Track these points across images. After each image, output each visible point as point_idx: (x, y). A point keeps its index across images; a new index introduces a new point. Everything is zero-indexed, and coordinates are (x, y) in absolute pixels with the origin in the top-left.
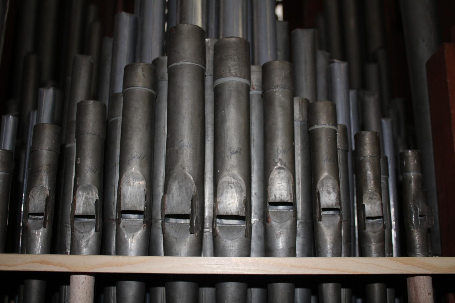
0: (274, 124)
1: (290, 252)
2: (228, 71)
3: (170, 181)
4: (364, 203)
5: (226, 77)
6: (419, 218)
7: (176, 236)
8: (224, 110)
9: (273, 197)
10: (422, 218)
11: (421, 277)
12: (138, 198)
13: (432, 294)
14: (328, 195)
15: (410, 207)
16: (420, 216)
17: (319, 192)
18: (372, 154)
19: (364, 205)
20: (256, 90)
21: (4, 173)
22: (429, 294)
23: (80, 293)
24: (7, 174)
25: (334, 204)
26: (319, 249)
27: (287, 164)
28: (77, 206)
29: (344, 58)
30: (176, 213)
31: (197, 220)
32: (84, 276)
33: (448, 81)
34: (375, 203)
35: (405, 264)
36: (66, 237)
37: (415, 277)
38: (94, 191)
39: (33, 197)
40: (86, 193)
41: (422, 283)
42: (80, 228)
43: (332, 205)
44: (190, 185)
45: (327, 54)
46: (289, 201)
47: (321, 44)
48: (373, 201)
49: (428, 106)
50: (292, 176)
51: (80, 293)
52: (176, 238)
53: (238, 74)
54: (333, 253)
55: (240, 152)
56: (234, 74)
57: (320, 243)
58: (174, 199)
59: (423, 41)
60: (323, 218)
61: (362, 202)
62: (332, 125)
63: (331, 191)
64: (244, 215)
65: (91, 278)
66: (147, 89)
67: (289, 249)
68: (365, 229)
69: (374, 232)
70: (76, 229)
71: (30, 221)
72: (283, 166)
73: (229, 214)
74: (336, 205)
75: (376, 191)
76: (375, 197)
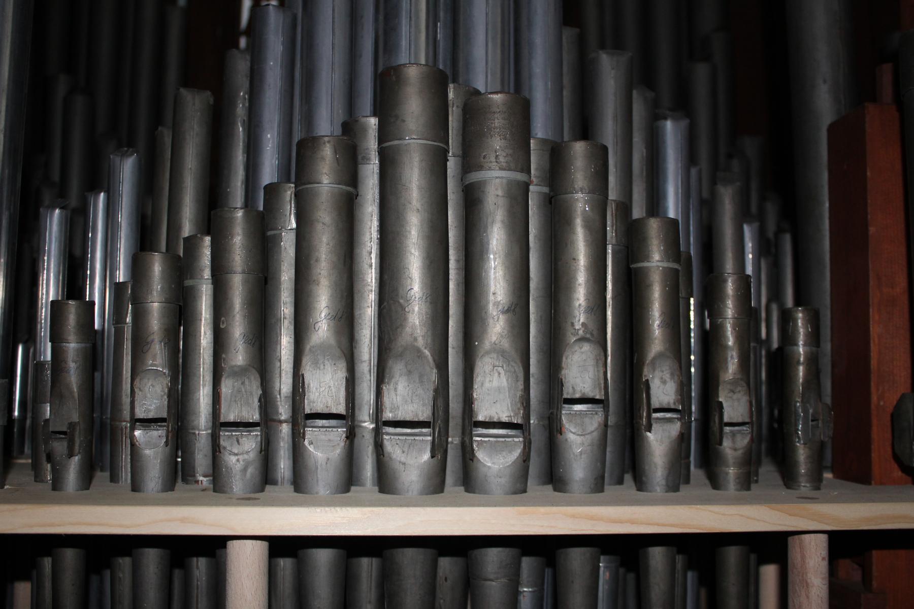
0: (574, 259)
1: (596, 484)
2: (493, 159)
3: (390, 363)
4: (720, 400)
5: (490, 169)
6: (810, 423)
7: (403, 459)
8: (485, 231)
9: (571, 390)
10: (814, 423)
11: (812, 535)
12: (334, 390)
13: (827, 559)
14: (662, 386)
15: (795, 406)
16: (812, 421)
17: (647, 380)
18: (739, 315)
19: (721, 403)
20: (536, 185)
21: (83, 345)
22: (823, 559)
23: (246, 571)
24: (88, 345)
25: (672, 401)
26: (644, 479)
27: (595, 333)
28: (439, 595)
29: (682, 105)
30: (402, 419)
31: (439, 432)
32: (254, 542)
33: (868, 174)
34: (738, 400)
35: (790, 515)
36: (194, 453)
37: (803, 536)
38: (252, 378)
39: (140, 390)
40: (240, 382)
41: (813, 543)
42: (232, 445)
43: (669, 403)
44: (428, 369)
45: (650, 95)
46: (598, 397)
47: (642, 75)
48: (735, 397)
49: (827, 205)
50: (602, 354)
51: (246, 571)
52: (404, 464)
53: (512, 165)
54: (667, 485)
55: (514, 310)
56: (504, 164)
57: (647, 468)
58: (398, 392)
59: (825, 82)
60: (654, 426)
61: (718, 397)
62: (674, 261)
63: (668, 380)
64: (520, 421)
65: (265, 544)
66: (344, 187)
67: (596, 479)
68: (721, 444)
69: (735, 450)
70: (225, 448)
71: (137, 433)
72: (588, 336)
73: (495, 420)
74: (674, 403)
75: (741, 379)
76: (739, 388)
